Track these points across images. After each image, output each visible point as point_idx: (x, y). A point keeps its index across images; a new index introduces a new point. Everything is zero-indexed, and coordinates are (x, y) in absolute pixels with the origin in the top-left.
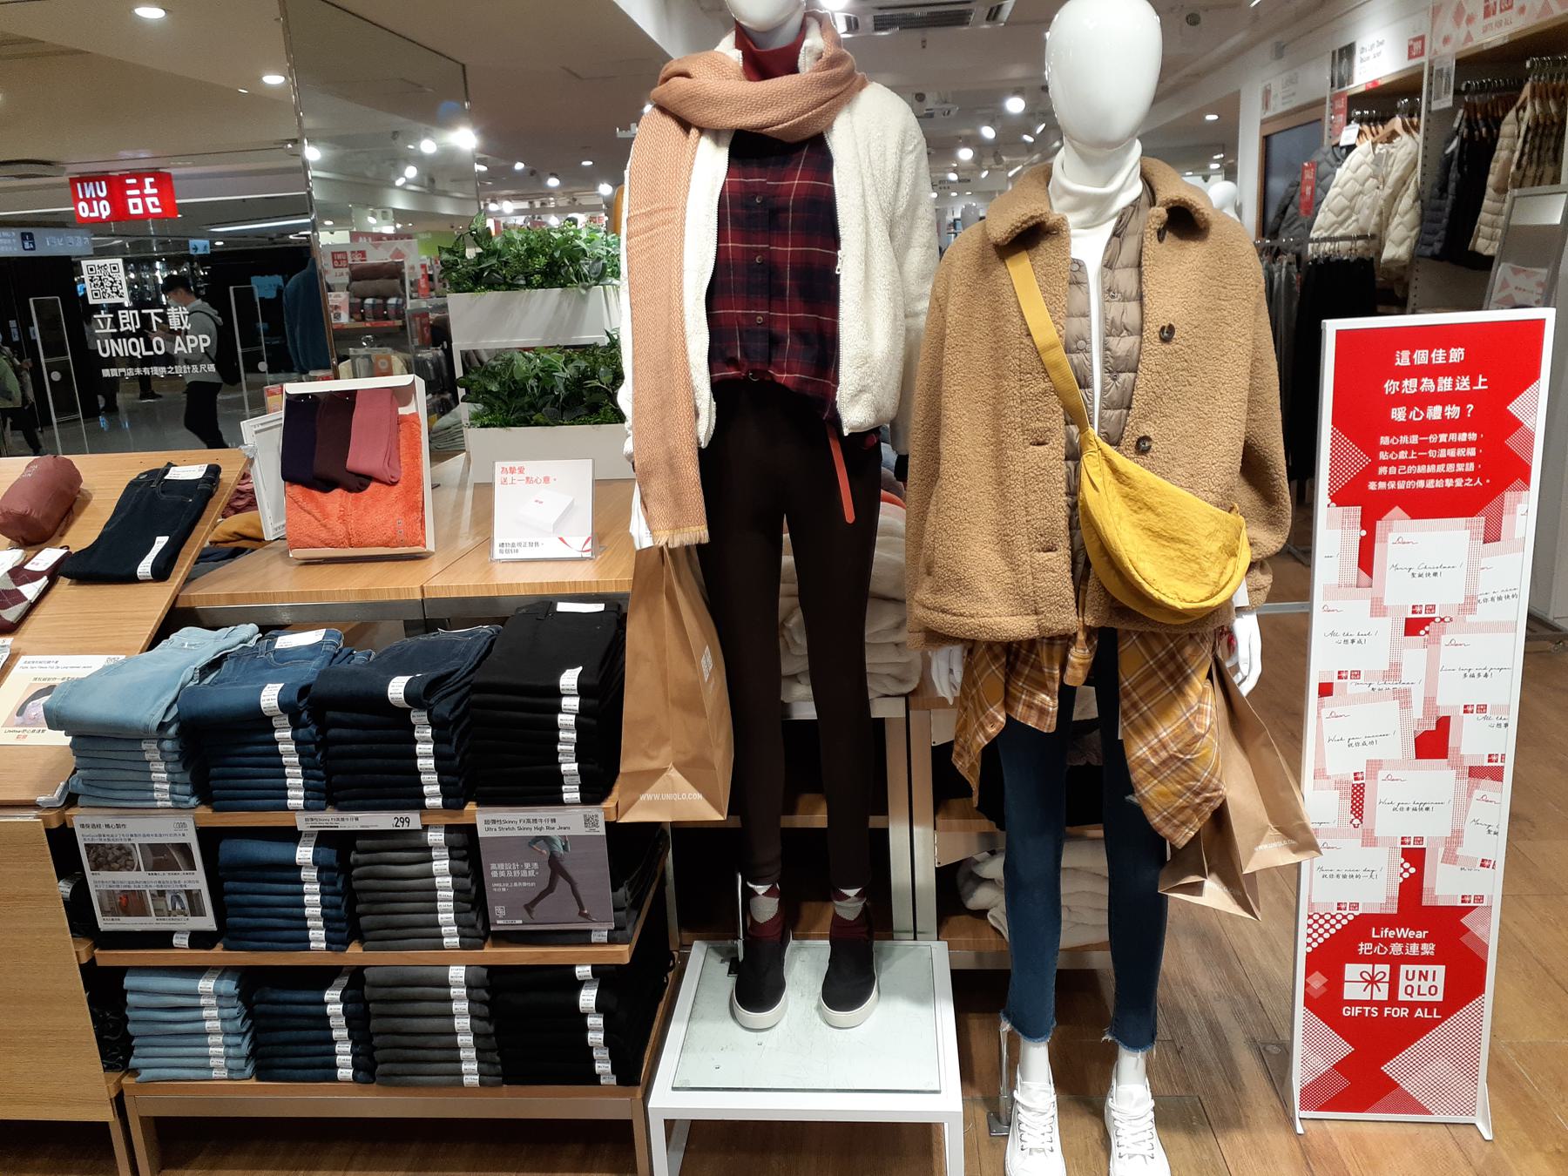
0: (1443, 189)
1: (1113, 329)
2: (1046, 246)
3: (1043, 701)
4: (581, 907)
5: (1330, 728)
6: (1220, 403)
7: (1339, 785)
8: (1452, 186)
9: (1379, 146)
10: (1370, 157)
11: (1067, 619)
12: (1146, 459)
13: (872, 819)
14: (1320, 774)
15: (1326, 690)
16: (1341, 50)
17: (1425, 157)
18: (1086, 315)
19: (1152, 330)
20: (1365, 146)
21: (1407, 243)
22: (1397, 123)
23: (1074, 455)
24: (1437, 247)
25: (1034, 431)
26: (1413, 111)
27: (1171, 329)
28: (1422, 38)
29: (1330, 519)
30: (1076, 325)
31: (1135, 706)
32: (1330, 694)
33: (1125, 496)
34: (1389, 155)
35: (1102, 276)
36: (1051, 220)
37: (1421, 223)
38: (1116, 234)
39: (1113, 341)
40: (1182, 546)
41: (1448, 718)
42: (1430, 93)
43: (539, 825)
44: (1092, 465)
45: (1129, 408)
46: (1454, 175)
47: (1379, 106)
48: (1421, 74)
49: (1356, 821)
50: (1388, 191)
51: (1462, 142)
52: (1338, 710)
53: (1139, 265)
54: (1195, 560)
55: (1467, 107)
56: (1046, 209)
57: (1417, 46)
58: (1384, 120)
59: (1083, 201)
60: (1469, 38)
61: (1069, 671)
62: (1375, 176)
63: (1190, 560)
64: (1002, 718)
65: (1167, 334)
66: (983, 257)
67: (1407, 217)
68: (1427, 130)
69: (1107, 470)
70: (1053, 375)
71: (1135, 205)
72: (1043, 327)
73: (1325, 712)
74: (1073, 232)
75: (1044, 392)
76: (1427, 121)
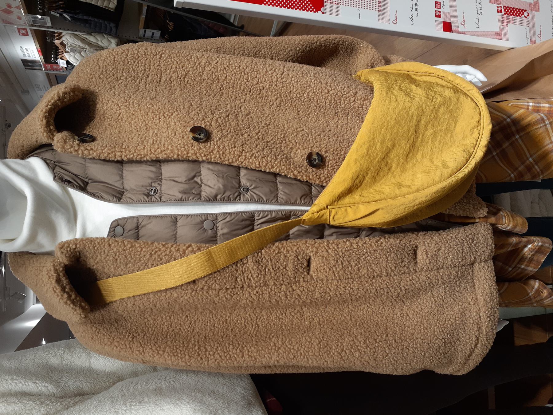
0: (86, 22)
1: (192, 192)
2: (94, 262)
3: (531, 250)
5: (470, 26)
6: (267, 84)
7: (505, 23)
8: (85, 17)
9: (67, 50)
10: (72, 54)
11: (481, 232)
12: (329, 158)
14: (498, 36)
15: (447, 27)
16: (24, 65)
17: (72, 30)
18: (174, 219)
19: (195, 150)
20: (66, 56)
21: (110, 39)
22: (57, 42)
23: (319, 229)
24: (112, 25)
25: (296, 270)
26: (52, 35)
27: (195, 130)
28: (19, 29)
29: (332, 13)
30: (184, 231)
31: (529, 168)
32: (450, 24)
33: (375, 179)
34: (71, 46)
35: (131, 202)
36: (62, 259)
37: (102, 33)
38: (83, 188)
39: (206, 191)
40: (423, 122)
42: (43, 27)
44: (349, 214)
45: (276, 175)
46: (80, 16)
47: (49, 50)
48: (35, 30)
49: (525, 14)
50: (87, 47)
51: (65, 12)
52: (460, 20)
53: (121, 162)
54: (435, 110)
55: (50, 9)
56: (48, 265)
57: (22, 31)
58: (57, 48)
59: (43, 221)
60: (18, 8)
61: (518, 230)
62: (80, 52)
63: (436, 116)
64: (537, 284)
65: (201, 134)
66: (102, 322)
67: (99, 39)
68: (60, 29)
69: (347, 200)
70: (240, 255)
71: (52, 165)
72: (188, 267)
73: (461, 29)
74: (78, 236)
75: (258, 262)
76: (56, 28)
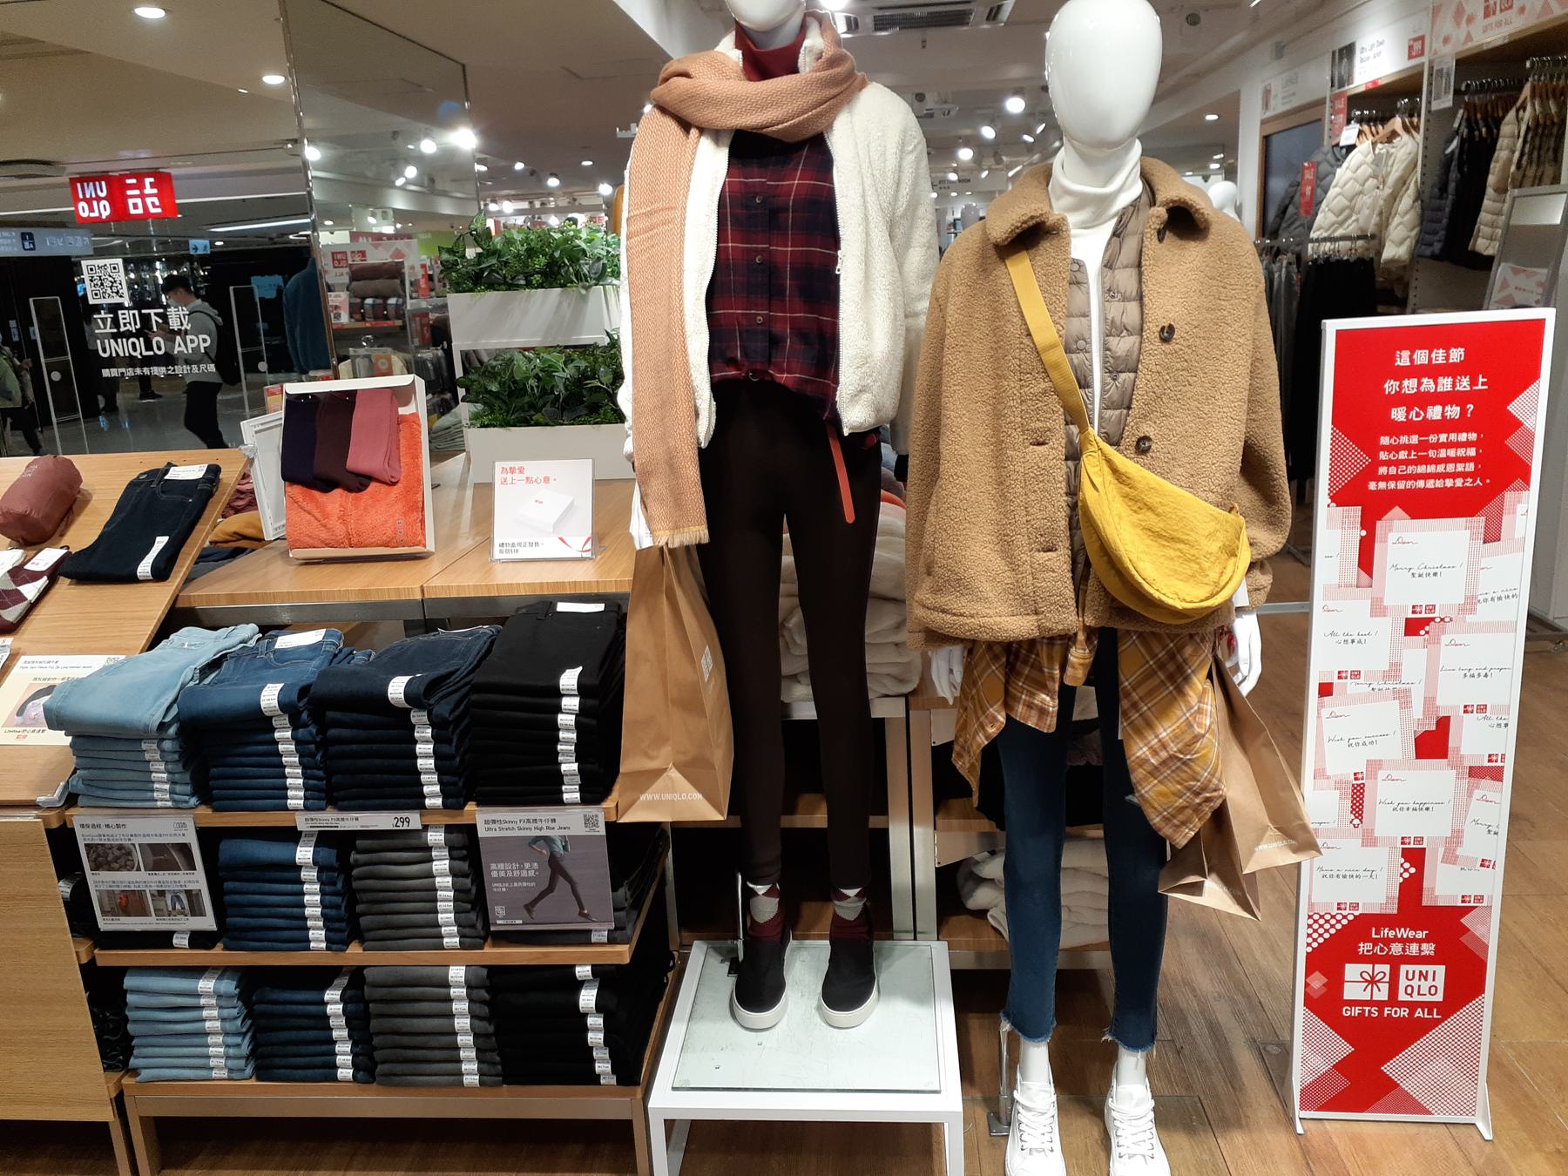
0: (1443, 189)
1: (1113, 329)
2: (1046, 246)
3: (1043, 701)
4: (581, 907)
5: (1330, 728)
6: (1220, 403)
7: (1339, 785)
8: (1452, 186)
9: (1379, 146)
10: (1370, 157)
11: (1067, 619)
12: (1146, 459)
13: (872, 819)
14: (1320, 774)
15: (1326, 690)
16: (1341, 50)
17: (1425, 157)
18: (1086, 315)
19: (1152, 330)
20: (1365, 146)
21: (1407, 243)
22: (1397, 123)
23: (1074, 455)
24: (1437, 247)
25: (1034, 431)
26: (1413, 111)
27: (1171, 329)
28: (1422, 38)
29: (1330, 519)
30: (1076, 325)
31: (1135, 706)
32: (1330, 694)
33: (1125, 496)
34: (1389, 155)
35: (1102, 276)
36: (1051, 220)
37: (1421, 223)
38: (1116, 234)
39: (1113, 341)
40: (1182, 546)
41: (1448, 718)
42: (1430, 93)
43: (539, 825)
44: (1092, 465)
45: (1129, 408)
46: (1454, 175)
47: (1379, 106)
48: (1421, 74)
49: (1356, 821)
50: (1388, 191)
51: (1462, 142)
52: (1338, 710)
53: (1139, 265)
54: (1195, 560)
55: (1467, 107)
56: (1046, 209)
57: (1417, 46)
58: (1384, 120)
59: (1083, 201)
60: (1469, 38)
61: (1069, 671)
62: (1375, 176)
63: (1190, 560)
64: (1002, 718)
65: (1167, 334)
66: (983, 257)
67: (1407, 217)
68: (1427, 130)
69: (1107, 470)
70: (1053, 375)
71: (1135, 205)
72: (1043, 327)
73: (1325, 712)
74: (1073, 232)
75: (1044, 392)
76: (1427, 121)
